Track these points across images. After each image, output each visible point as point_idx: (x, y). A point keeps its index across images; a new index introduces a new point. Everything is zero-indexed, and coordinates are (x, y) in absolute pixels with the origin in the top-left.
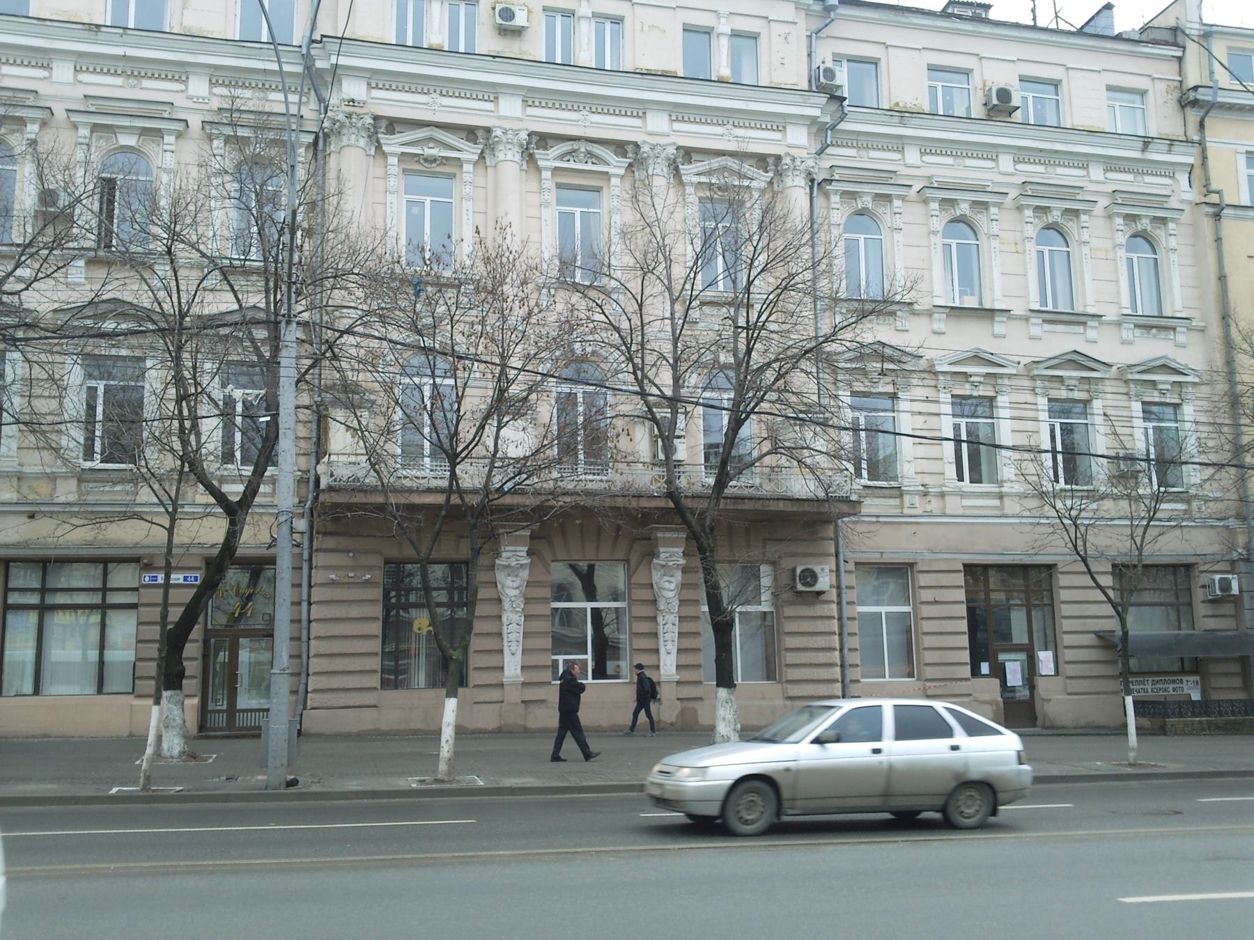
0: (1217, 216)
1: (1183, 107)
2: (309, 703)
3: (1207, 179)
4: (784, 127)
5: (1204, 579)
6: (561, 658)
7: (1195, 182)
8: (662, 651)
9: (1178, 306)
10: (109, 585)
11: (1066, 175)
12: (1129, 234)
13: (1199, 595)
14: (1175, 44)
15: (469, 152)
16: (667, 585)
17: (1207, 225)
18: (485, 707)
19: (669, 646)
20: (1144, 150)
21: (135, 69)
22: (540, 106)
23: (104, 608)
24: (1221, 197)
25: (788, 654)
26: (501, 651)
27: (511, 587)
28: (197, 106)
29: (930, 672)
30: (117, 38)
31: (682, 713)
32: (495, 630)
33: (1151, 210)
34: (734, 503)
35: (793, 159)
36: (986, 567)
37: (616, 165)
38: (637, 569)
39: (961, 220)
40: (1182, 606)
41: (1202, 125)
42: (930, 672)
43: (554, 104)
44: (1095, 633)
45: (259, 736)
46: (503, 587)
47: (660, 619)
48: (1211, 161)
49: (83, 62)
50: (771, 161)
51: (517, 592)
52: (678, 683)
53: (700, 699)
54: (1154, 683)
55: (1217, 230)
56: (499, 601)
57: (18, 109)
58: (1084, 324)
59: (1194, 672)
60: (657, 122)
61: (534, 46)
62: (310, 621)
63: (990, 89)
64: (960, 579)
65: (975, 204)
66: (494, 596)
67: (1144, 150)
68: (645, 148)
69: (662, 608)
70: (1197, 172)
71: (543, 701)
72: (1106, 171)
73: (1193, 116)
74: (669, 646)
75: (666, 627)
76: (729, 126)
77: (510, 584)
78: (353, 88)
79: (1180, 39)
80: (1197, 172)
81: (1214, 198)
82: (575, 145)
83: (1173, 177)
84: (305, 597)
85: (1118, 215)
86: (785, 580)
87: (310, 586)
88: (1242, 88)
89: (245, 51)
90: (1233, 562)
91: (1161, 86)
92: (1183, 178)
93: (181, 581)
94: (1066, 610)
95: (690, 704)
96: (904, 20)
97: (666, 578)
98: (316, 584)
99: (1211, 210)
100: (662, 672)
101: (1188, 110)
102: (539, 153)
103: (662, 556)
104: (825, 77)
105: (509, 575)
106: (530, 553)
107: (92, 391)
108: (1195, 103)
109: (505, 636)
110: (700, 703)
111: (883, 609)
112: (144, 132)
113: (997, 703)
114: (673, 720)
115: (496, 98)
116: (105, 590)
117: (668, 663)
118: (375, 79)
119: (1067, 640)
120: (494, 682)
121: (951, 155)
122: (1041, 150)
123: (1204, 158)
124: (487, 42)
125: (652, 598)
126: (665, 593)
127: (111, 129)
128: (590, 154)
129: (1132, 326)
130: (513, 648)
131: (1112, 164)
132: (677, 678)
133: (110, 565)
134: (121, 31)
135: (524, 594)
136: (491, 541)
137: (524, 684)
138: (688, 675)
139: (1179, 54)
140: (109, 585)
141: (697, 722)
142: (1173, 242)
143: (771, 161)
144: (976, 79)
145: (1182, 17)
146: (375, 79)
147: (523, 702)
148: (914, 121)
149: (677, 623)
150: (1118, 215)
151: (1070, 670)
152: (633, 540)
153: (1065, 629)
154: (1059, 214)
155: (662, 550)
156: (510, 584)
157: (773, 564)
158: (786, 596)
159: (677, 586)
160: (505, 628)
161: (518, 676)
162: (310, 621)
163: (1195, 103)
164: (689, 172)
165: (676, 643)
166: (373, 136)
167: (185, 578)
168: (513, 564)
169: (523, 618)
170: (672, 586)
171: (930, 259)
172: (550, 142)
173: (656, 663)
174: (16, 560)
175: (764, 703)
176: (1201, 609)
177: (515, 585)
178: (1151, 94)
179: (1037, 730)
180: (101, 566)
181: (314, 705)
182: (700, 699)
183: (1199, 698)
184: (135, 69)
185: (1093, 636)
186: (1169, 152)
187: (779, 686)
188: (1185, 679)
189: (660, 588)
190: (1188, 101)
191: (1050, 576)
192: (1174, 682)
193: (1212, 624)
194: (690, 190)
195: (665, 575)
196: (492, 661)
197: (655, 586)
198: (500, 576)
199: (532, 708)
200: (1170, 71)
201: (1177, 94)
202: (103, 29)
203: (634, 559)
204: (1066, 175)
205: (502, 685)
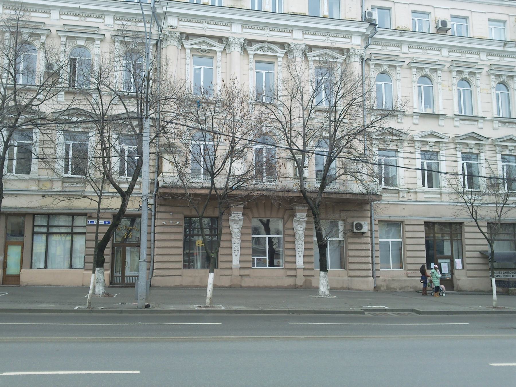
2: (154, 274)
6: (256, 258)
8: (297, 256)
10: (74, 225)
12: (497, 83)
15: (220, 47)
16: (299, 229)
18: (225, 277)
19: (300, 254)
23: (72, 234)
25: (350, 258)
26: (231, 254)
27: (235, 228)
31: (305, 281)
32: (229, 246)
34: (328, 195)
35: (355, 50)
36: (434, 223)
37: (280, 53)
38: (287, 221)
44: (479, 251)
46: (232, 228)
47: (296, 243)
51: (238, 230)
52: (304, 269)
53: (313, 276)
56: (231, 234)
58: (477, 121)
60: (298, 35)
62: (154, 241)
63: (438, 21)
64: (423, 228)
65: (390, 66)
66: (294, 267)
68: (292, 46)
69: (297, 238)
71: (248, 275)
72: (487, 56)
74: (300, 254)
75: (299, 246)
76: (328, 36)
77: (235, 227)
78: (172, 21)
82: (263, 44)
84: (153, 231)
85: (493, 74)
86: (349, 227)
87: (155, 226)
93: (103, 223)
94: (467, 242)
95: (309, 278)
97: (299, 226)
98: (157, 226)
100: (297, 264)
102: (248, 48)
103: (298, 216)
105: (235, 223)
106: (243, 214)
107: (67, 146)
109: (233, 248)
110: (312, 278)
111: (390, 240)
112: (88, 39)
114: (302, 284)
115: (231, 25)
117: (300, 261)
119: (468, 254)
120: (228, 267)
121: (422, 49)
125: (293, 234)
126: (298, 232)
127: (74, 38)
128: (270, 48)
129: (498, 122)
130: (236, 253)
131: (490, 53)
132: (303, 267)
135: (241, 231)
136: (228, 209)
137: (240, 268)
140: (74, 225)
141: (311, 285)
147: (240, 275)
149: (303, 244)
150: (493, 74)
152: (286, 210)
154: (467, 74)
155: (297, 214)
156: (235, 227)
157: (344, 220)
159: (304, 229)
160: (233, 245)
161: (238, 265)
162: (154, 241)
164: (311, 55)
165: (303, 253)
166: (180, 41)
167: (105, 222)
168: (237, 219)
169: (240, 241)
170: (302, 229)
172: (253, 43)
173: (295, 261)
175: (339, 278)
177: (237, 227)
178: (508, 22)
181: (156, 275)
182: (313, 276)
185: (478, 253)
187: (346, 271)
189: (297, 230)
191: (461, 227)
195: (299, 224)
196: (227, 258)
197: (294, 229)
199: (244, 278)
203: (286, 217)
204: (470, 58)
205: (232, 268)
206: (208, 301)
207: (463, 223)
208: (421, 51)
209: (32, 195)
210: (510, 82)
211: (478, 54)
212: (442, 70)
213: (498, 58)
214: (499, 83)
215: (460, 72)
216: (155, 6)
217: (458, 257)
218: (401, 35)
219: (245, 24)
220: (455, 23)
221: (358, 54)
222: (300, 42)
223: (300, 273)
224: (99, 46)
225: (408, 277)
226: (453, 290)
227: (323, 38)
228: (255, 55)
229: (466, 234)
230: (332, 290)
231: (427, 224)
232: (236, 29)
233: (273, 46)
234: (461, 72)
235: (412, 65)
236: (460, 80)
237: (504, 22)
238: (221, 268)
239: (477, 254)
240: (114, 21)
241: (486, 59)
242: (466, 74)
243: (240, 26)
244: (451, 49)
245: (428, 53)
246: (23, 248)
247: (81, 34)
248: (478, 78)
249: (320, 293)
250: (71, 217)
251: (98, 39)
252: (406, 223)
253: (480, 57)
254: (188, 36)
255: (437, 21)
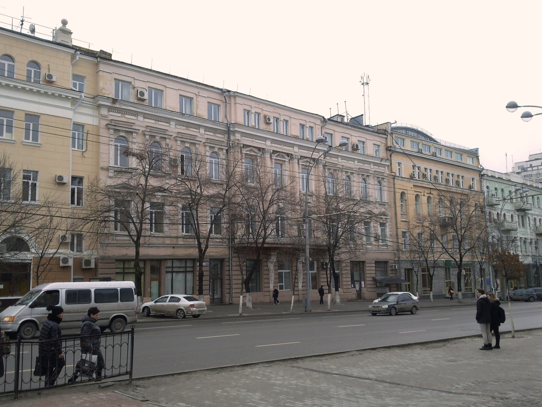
0: (394, 179)
1: (387, 150)
2: (233, 296)
3: (392, 169)
4: (137, 115)
5: (390, 265)
7: (389, 170)
9: (386, 200)
10: (174, 266)
11: (192, 131)
12: (211, 152)
13: (389, 269)
14: (385, 134)
17: (392, 180)
20: (381, 161)
21: (188, 125)
22: (113, 112)
23: (172, 272)
24: (395, 174)
25: (321, 283)
27: (271, 266)
28: (202, 137)
29: (345, 287)
30: (187, 117)
33: (160, 134)
35: (268, 149)
37: (287, 159)
39: (216, 153)
40: (385, 272)
41: (391, 156)
42: (345, 287)
43: (118, 111)
44: (372, 277)
45: (321, 304)
48: (393, 165)
49: (179, 123)
50: (290, 155)
52: (302, 290)
54: (382, 289)
55: (394, 182)
57: (116, 127)
58: (370, 203)
59: (388, 287)
60: (296, 149)
61: (271, 128)
62: (232, 275)
63: (354, 144)
64: (374, 265)
65: (219, 148)
67: (381, 161)
70: (389, 166)
72: (342, 159)
73: (389, 153)
76: (283, 146)
78: (238, 136)
79: (386, 133)
80: (389, 167)
81: (394, 174)
83: (385, 168)
84: (231, 269)
85: (112, 129)
86: (320, 264)
87: (232, 266)
88: (399, 148)
89: (215, 124)
90: (395, 261)
91: (383, 144)
92: (387, 168)
93: (205, 265)
94: (368, 272)
96: (338, 125)
98: (234, 266)
99: (393, 177)
101: (388, 151)
104: (47, 77)
108: (390, 150)
111: (283, 271)
112: (126, 132)
113: (356, 294)
115: (266, 141)
116: (173, 267)
118: (244, 134)
119: (368, 279)
121: (213, 132)
122: (363, 160)
123: (391, 164)
124: (263, 126)
127: (119, 130)
128: (282, 156)
131: (375, 164)
132: (302, 289)
133: (174, 261)
134: (189, 116)
136: (268, 256)
138: (305, 288)
139: (386, 137)
142: (385, 184)
143: (290, 155)
144: (350, 140)
145: (387, 128)
146: (244, 134)
148: (342, 152)
150: (112, 129)
151: (368, 286)
153: (367, 276)
154: (217, 149)
158: (321, 269)
162: (232, 275)
163: (390, 150)
167: (206, 264)
171: (109, 150)
174: (188, 259)
176: (390, 272)
178: (381, 146)
179: (362, 300)
180: (172, 261)
181: (235, 296)
183: (3, 285)
184: (188, 125)
186: (385, 162)
188: (387, 288)
190: (388, 149)
191: (363, 264)
192: (384, 289)
193: (392, 275)
194: (273, 160)
196: (267, 285)
198: (269, 264)
200: (384, 141)
201: (385, 147)
202: (185, 115)
204: (192, 131)
206: (329, 307)
207: (365, 261)
208: (346, 161)
209: (168, 247)
210: (351, 176)
211: (198, 129)
212: (199, 144)
213: (153, 121)
214: (330, 173)
215: (346, 172)
216: (230, 126)
217: (88, 280)
218: (339, 152)
219: (273, 141)
220: (33, 70)
221: (297, 158)
222: (297, 154)
223: (301, 293)
224: (135, 137)
225: (344, 293)
226: (361, 299)
227: (307, 152)
228: (303, 165)
229: (367, 268)
230: (342, 301)
231: (376, 262)
232: (268, 143)
233: (283, 154)
234: (154, 136)
235: (207, 144)
236: (212, 153)
237: (379, 146)
238: (265, 291)
239: (371, 279)
240: (108, 112)
241: (142, 121)
242: (332, 170)
243: (270, 142)
244: (360, 161)
245: (126, 117)
246: (160, 283)
247: (190, 140)
248: (134, 137)
249: (337, 303)
250: (172, 261)
251: (355, 173)
252: (366, 262)
253: (354, 163)
254: (245, 146)
255: (353, 143)
